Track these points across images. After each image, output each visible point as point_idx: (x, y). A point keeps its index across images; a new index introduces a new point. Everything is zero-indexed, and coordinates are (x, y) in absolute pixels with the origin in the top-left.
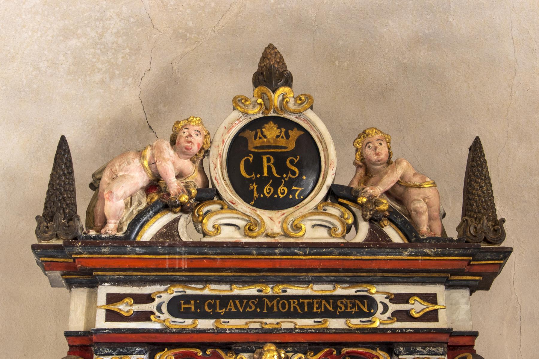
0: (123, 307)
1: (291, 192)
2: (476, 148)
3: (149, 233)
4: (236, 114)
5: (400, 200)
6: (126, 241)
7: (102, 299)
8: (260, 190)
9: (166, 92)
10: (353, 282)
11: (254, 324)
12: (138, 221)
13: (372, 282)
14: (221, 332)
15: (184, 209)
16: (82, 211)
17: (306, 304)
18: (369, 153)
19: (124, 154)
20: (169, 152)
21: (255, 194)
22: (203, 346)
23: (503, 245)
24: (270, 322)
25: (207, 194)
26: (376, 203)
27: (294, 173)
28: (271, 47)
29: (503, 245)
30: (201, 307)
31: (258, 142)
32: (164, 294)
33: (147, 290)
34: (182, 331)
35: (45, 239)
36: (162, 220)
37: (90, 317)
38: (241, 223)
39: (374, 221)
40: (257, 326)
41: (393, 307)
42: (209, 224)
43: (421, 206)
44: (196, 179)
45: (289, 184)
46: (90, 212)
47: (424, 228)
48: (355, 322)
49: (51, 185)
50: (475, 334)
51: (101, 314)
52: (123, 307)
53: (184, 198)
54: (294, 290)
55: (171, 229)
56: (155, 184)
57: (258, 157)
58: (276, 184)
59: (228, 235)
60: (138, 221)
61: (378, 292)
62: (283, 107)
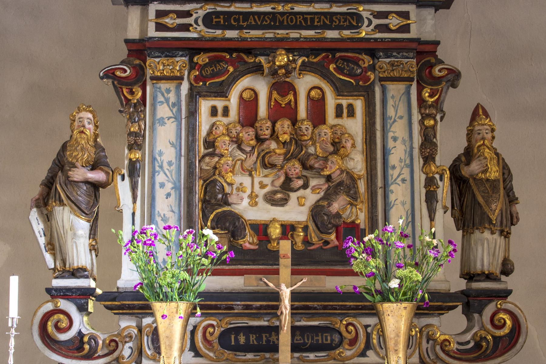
7: (152, 15)
11: (269, 34)
24: (281, 33)
40: (271, 35)
51: (152, 26)
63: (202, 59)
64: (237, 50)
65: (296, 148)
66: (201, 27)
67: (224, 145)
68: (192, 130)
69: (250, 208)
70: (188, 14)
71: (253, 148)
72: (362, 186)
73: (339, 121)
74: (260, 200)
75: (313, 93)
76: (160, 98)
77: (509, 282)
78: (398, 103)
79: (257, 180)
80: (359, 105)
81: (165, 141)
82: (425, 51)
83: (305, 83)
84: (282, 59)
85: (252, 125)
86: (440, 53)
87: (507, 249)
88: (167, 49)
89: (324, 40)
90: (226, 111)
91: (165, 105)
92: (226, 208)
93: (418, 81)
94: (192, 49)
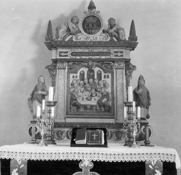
5: (117, 33)
7: (58, 53)
8: (89, 31)
11: (87, 58)
21: (88, 31)
23: (137, 42)
24: (91, 57)
27: (95, 27)
29: (137, 42)
30: (76, 54)
35: (47, 41)
40: (88, 58)
51: (58, 55)
56: (68, 30)
57: (88, 24)
58: (92, 30)
59: (82, 40)
60: (65, 37)
61: (112, 51)
63: (70, 63)
64: (79, 61)
66: (71, 56)
67: (76, 85)
68: (68, 81)
70: (67, 52)
71: (83, 86)
72: (110, 95)
73: (105, 79)
74: (85, 99)
75: (99, 72)
76: (60, 73)
77: (148, 120)
79: (84, 94)
80: (110, 75)
82: (127, 62)
83: (96, 70)
84: (90, 63)
85: (83, 80)
86: (131, 62)
87: (148, 112)
88: (62, 61)
89: (102, 59)
90: (76, 77)
91: (61, 75)
92: (76, 101)
93: (125, 70)
94: (68, 61)
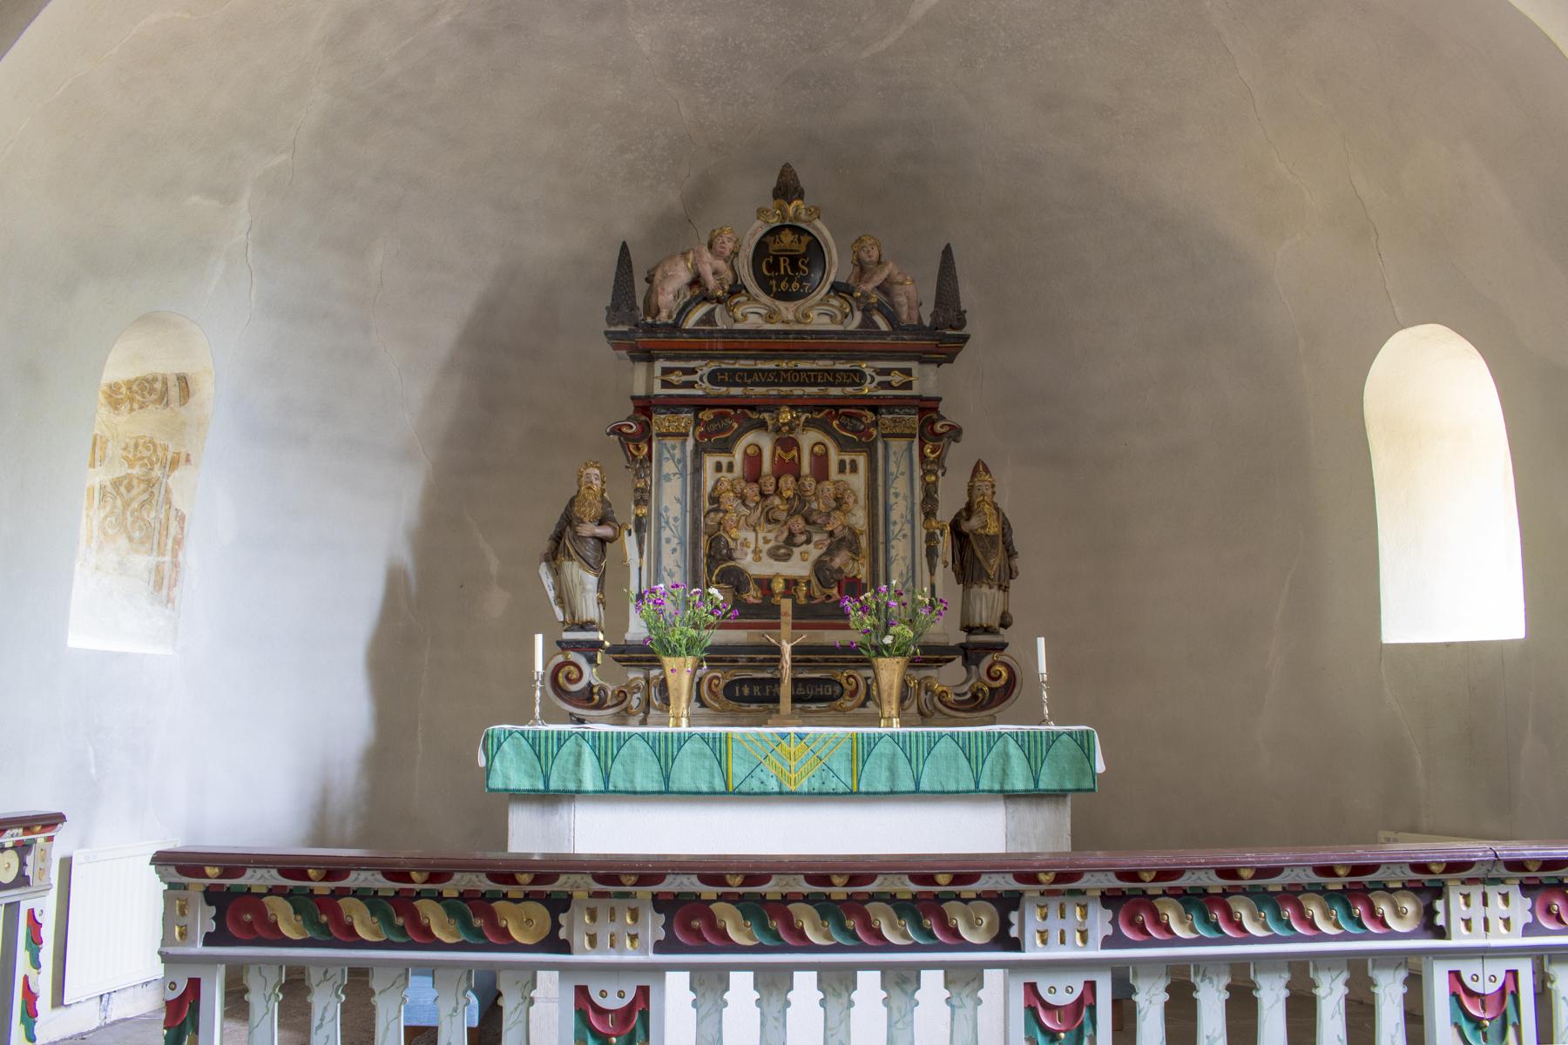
0: (673, 378)
1: (802, 287)
2: (947, 252)
3: (691, 322)
4: (759, 223)
6: (675, 327)
7: (658, 372)
8: (778, 286)
9: (702, 196)
10: (850, 359)
11: (773, 391)
12: (684, 311)
13: (863, 359)
14: (749, 397)
15: (719, 301)
16: (640, 303)
17: (804, 637)
18: (863, 255)
19: (671, 257)
20: (707, 256)
22: (735, 408)
24: (785, 390)
25: (736, 289)
26: (868, 297)
28: (787, 165)
30: (734, 378)
31: (776, 246)
32: (705, 368)
33: (692, 364)
34: (718, 397)
36: (703, 309)
37: (650, 386)
38: (763, 312)
39: (866, 311)
41: (879, 379)
42: (738, 313)
43: (902, 299)
44: (728, 275)
45: (800, 281)
46: (647, 301)
47: (904, 317)
48: (849, 390)
49: (616, 281)
50: (939, 399)
51: (657, 383)
52: (673, 378)
53: (720, 293)
54: (803, 365)
55: (708, 319)
57: (776, 258)
59: (754, 322)
60: (684, 311)
62: (796, 217)
65: (799, 504)
69: (754, 564)
78: (900, 458)
81: (671, 496)
82: (927, 408)
88: (673, 406)
94: (698, 406)
